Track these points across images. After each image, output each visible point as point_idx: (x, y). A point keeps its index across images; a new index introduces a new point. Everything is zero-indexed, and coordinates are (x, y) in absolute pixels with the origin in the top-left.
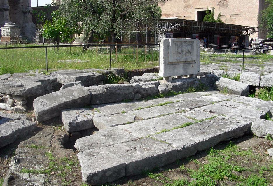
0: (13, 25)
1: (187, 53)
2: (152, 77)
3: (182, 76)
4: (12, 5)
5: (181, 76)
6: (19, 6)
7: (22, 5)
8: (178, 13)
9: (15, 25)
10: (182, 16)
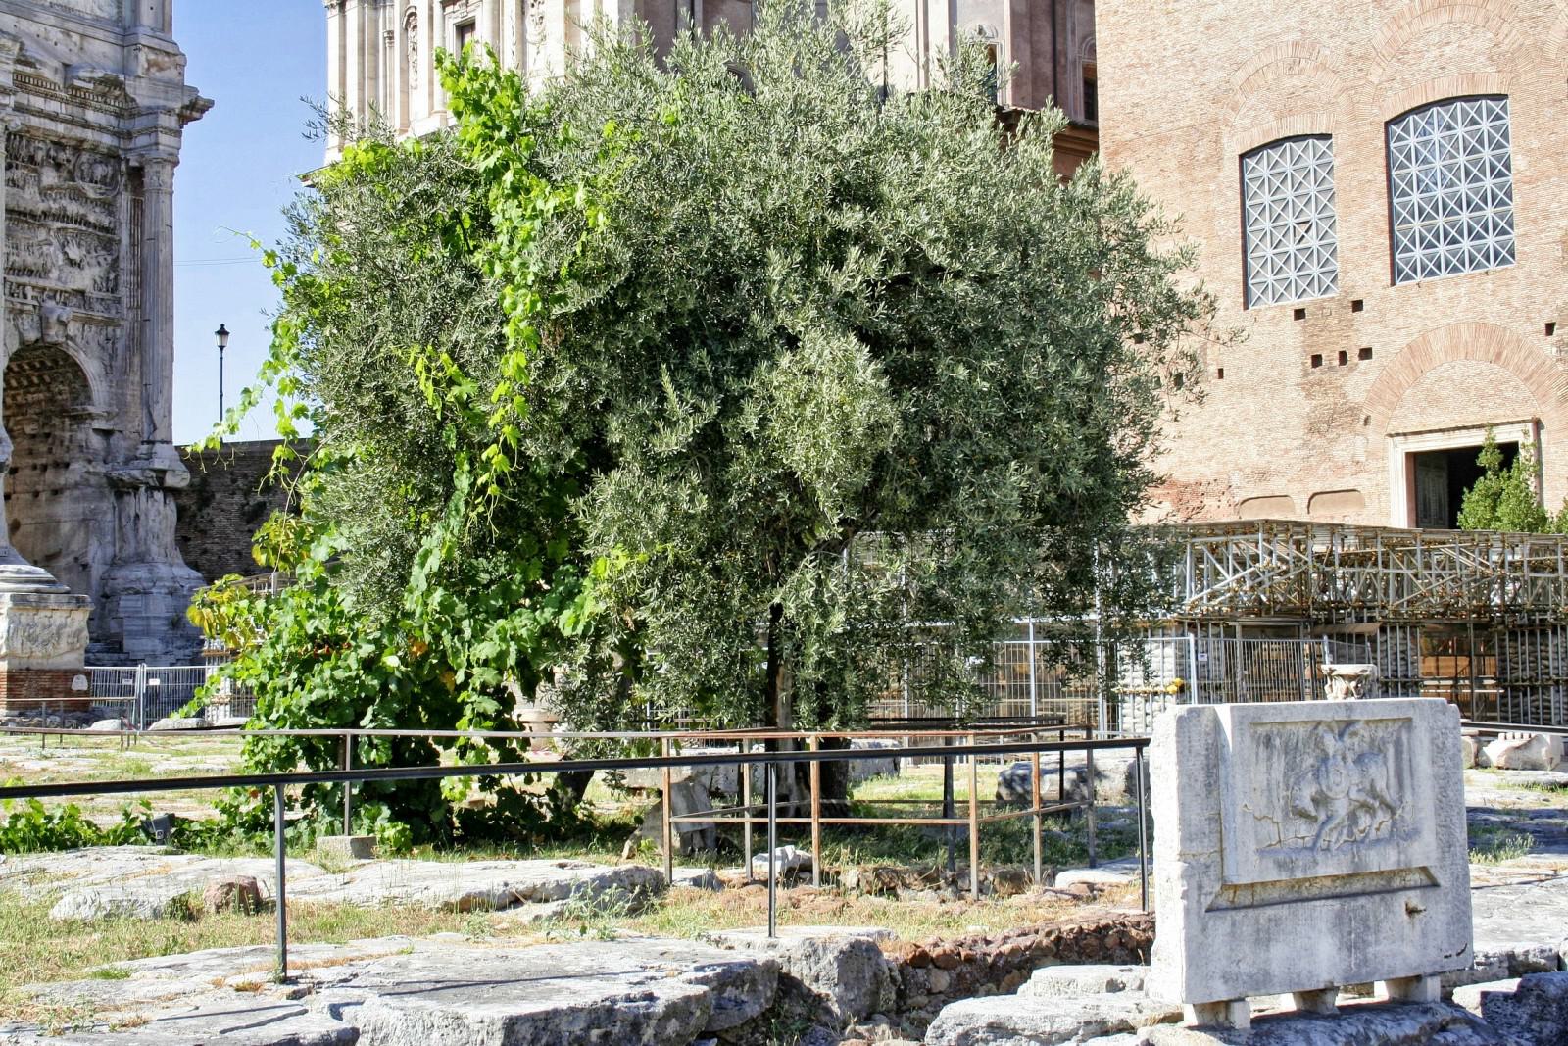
0: (27, 582)
1: (1361, 813)
2: (1090, 1000)
3: (1331, 989)
4: (29, 430)
5: (1323, 991)
6: (81, 436)
7: (106, 434)
8: (1264, 475)
9: (47, 582)
10: (1292, 489)
